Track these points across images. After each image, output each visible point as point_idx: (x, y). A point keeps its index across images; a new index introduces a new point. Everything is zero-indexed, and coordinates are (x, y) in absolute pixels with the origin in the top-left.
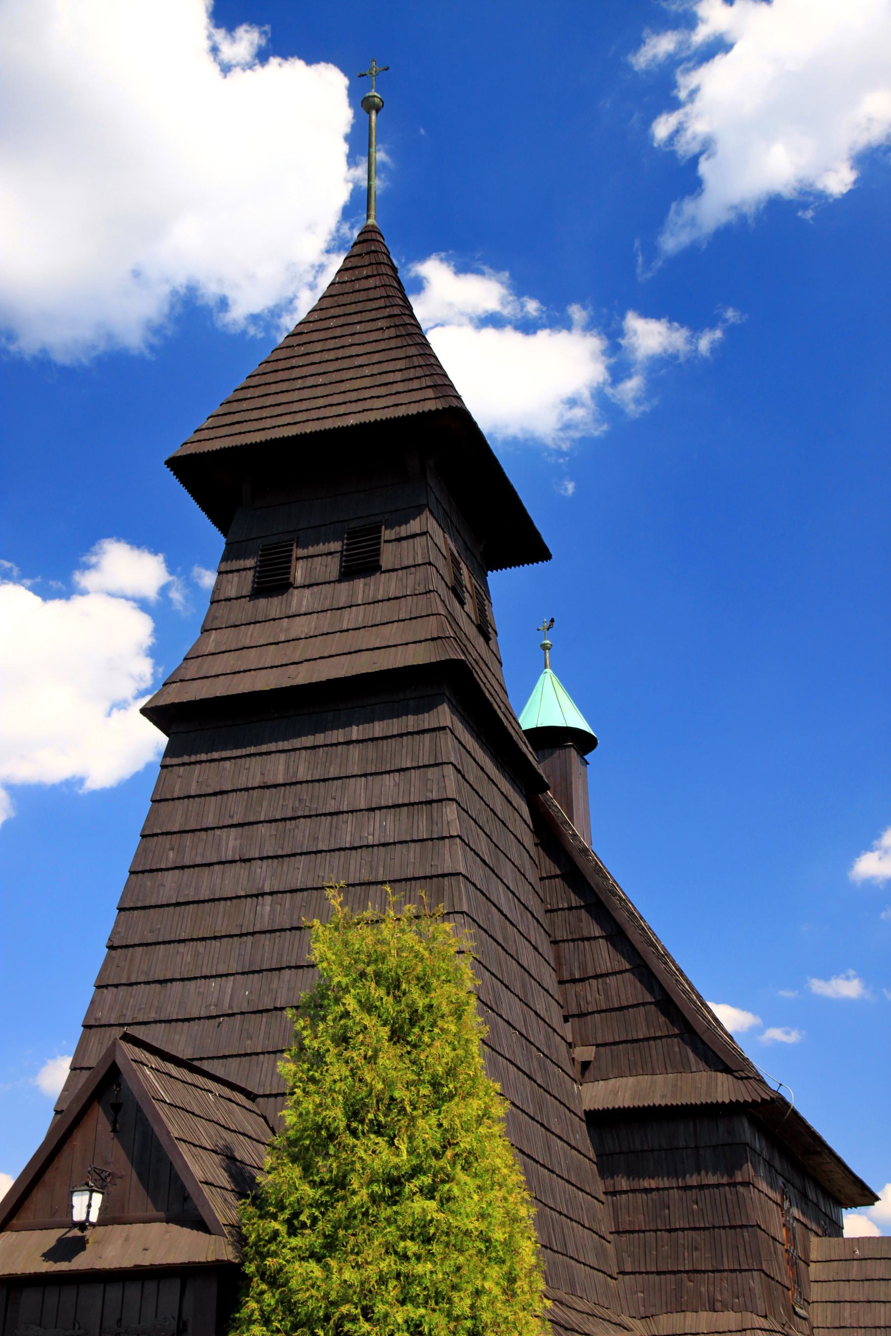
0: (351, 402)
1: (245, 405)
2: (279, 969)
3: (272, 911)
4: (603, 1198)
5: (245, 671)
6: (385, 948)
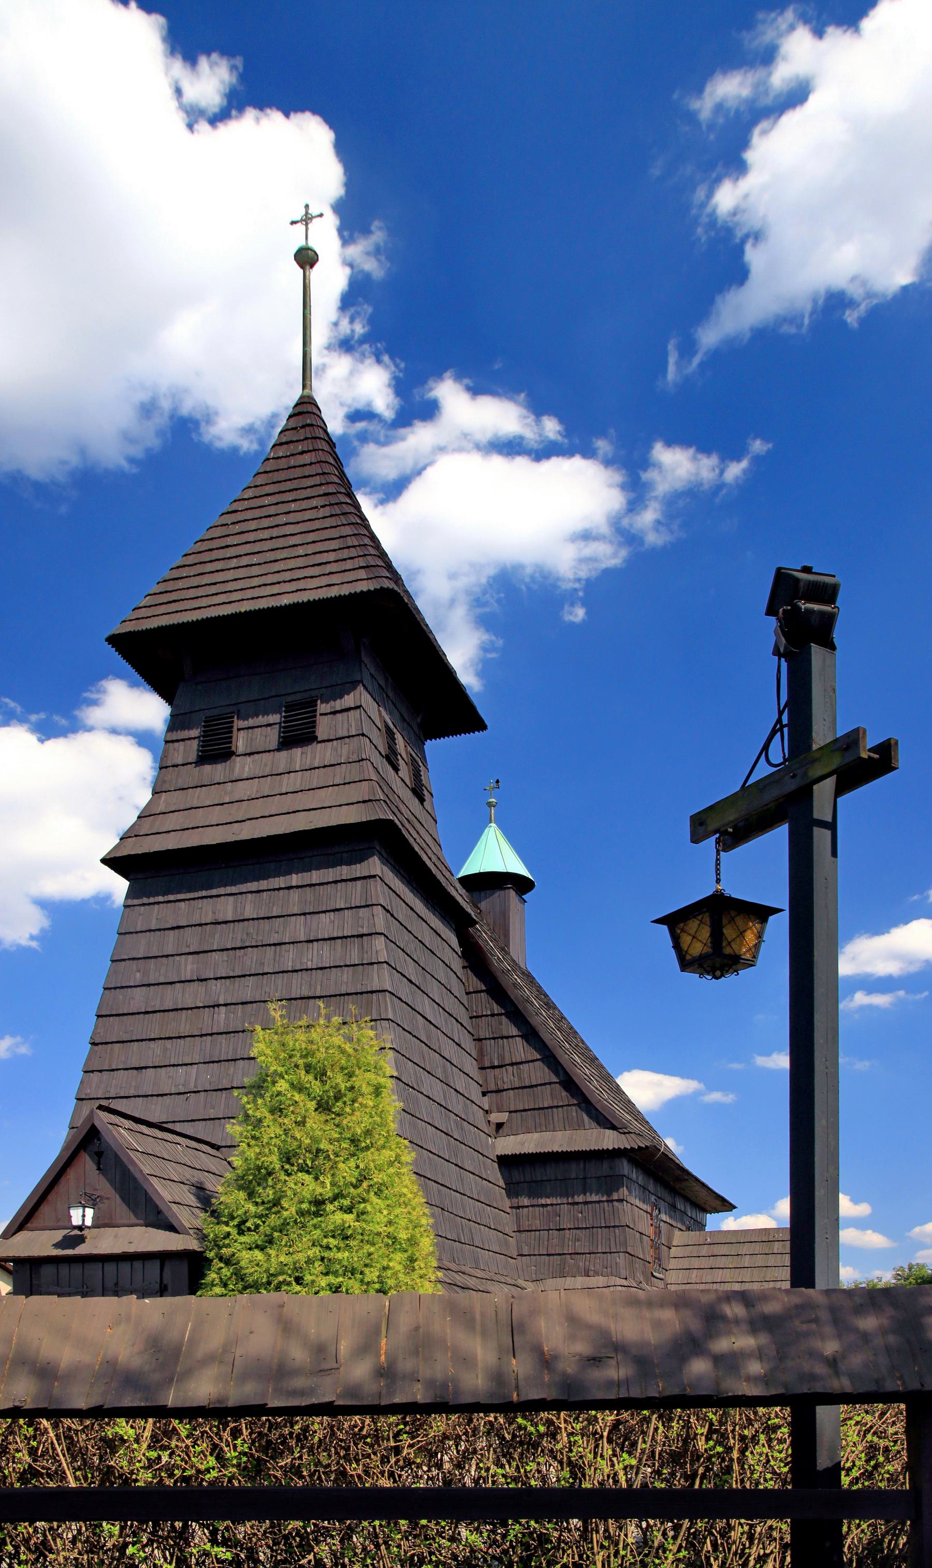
0: (285, 582)
1: (181, 584)
2: (235, 1060)
3: (227, 1018)
4: (509, 1210)
5: (193, 828)
6: (315, 1047)
